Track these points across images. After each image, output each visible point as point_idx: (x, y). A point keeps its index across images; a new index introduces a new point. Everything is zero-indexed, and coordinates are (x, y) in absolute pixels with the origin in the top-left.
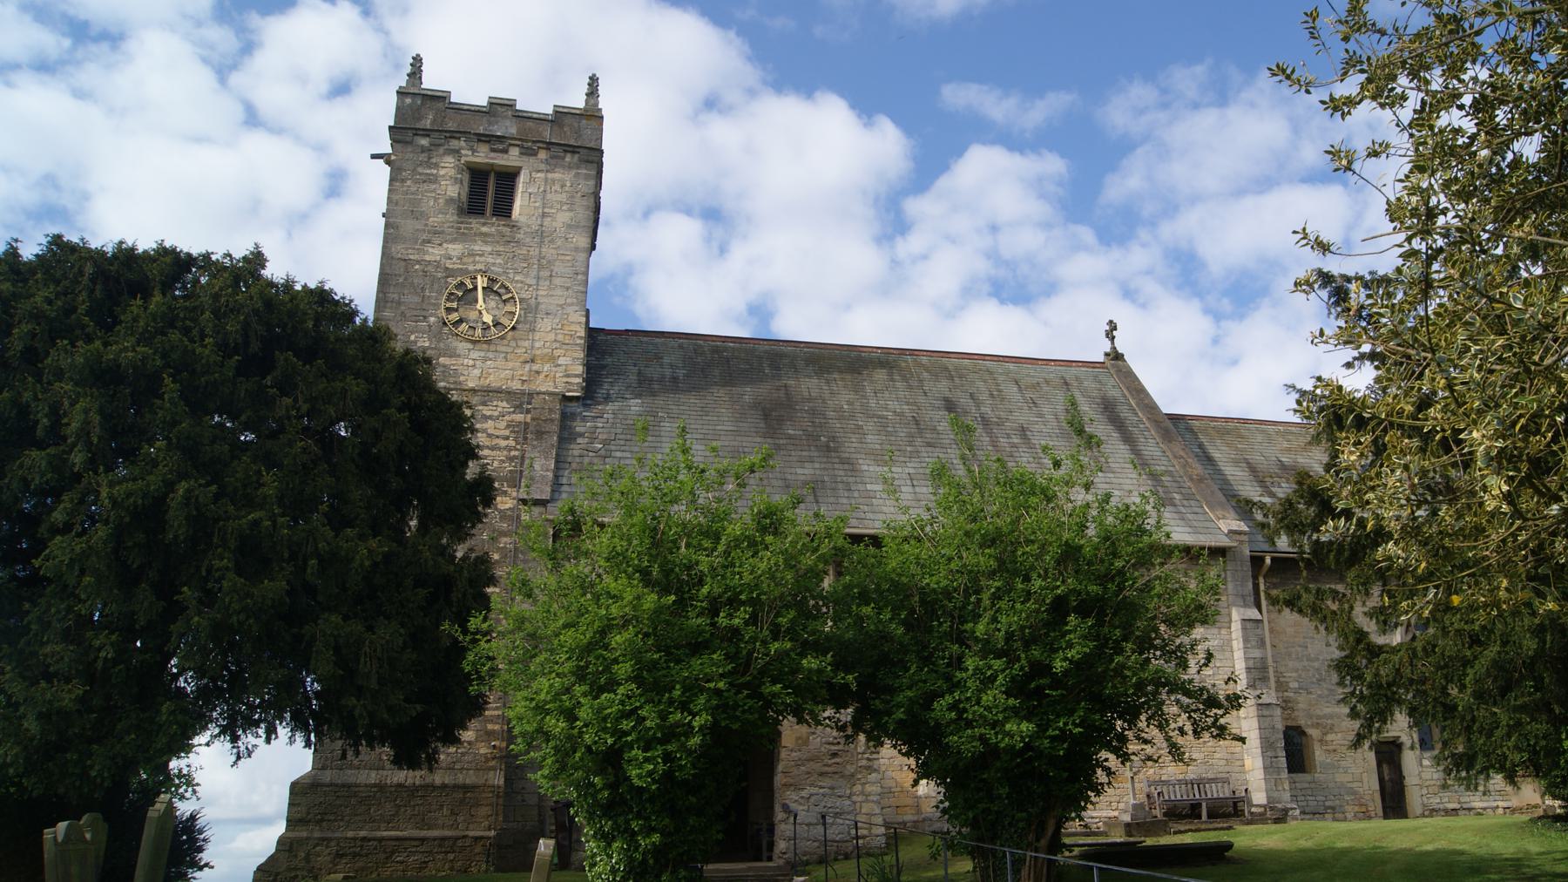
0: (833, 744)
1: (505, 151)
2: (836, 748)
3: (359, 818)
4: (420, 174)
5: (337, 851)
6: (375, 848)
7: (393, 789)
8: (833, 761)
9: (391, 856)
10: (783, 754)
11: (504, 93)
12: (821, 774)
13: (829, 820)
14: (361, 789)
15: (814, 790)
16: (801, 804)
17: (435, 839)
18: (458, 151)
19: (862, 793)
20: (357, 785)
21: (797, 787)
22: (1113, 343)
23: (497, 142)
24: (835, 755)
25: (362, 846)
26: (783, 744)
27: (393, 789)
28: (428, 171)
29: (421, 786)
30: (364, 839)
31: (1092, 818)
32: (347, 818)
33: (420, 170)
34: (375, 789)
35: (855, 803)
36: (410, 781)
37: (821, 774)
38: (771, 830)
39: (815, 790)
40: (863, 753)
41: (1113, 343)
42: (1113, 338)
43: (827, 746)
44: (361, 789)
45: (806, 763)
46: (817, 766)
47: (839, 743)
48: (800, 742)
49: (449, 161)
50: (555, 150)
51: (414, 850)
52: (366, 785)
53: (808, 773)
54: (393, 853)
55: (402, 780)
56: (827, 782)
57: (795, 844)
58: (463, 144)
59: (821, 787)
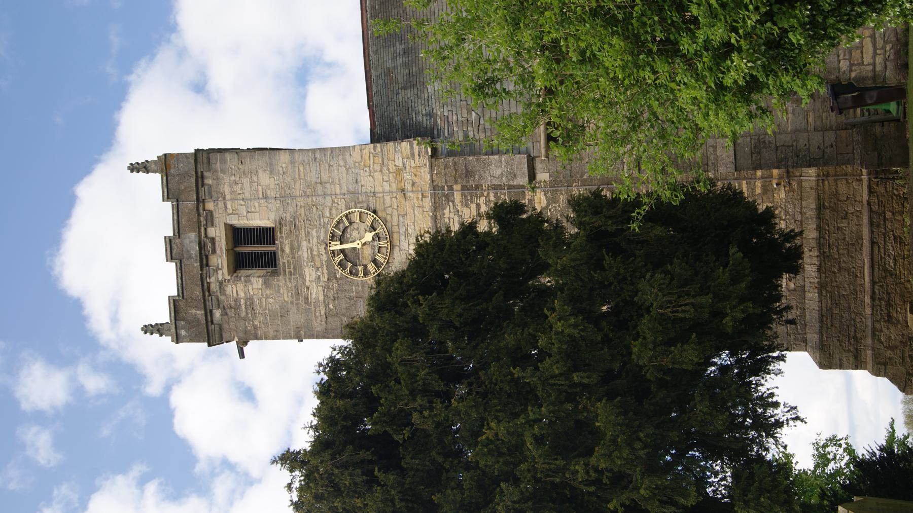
1: (213, 240)
3: (852, 305)
4: (247, 313)
6: (882, 286)
9: (890, 272)
14: (824, 305)
17: (872, 232)
18: (221, 283)
28: (243, 307)
29: (819, 250)
30: (873, 298)
32: (853, 315)
33: (243, 314)
44: (824, 305)
49: (230, 289)
51: (882, 251)
52: (821, 301)
54: (886, 270)
55: (814, 268)
58: (213, 279)
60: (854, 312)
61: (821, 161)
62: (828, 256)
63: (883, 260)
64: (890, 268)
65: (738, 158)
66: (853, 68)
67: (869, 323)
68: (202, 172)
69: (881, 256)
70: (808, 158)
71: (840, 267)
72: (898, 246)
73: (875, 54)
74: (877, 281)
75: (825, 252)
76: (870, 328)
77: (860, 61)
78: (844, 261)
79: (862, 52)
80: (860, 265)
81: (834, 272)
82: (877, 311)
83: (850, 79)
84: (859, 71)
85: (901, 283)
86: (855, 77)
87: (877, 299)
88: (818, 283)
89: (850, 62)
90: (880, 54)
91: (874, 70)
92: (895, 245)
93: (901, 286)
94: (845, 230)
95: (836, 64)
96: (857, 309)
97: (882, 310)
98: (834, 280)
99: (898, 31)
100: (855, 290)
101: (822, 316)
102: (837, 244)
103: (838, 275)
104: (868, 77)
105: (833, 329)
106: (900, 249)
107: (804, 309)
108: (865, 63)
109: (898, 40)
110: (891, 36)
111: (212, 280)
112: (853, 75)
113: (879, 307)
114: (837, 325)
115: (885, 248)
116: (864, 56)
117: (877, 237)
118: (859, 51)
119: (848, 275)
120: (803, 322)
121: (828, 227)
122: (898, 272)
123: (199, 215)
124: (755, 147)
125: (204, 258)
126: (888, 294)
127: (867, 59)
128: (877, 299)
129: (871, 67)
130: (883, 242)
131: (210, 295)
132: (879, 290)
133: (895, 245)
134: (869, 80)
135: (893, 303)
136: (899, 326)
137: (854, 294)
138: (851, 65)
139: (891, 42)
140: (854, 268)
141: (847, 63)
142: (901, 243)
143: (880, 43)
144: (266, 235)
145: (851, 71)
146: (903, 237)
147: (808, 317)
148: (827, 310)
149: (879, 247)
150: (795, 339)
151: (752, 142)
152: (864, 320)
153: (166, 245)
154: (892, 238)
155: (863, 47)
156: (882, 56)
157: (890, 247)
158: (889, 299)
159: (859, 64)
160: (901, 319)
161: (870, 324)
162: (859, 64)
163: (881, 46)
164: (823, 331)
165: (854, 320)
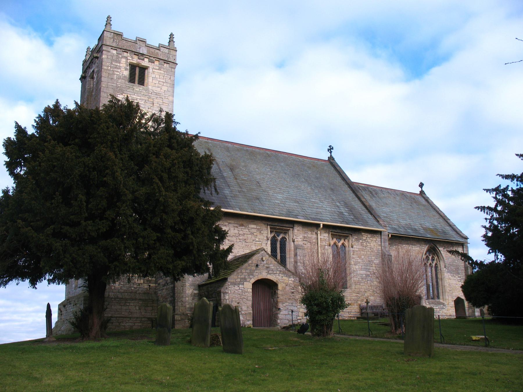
0: (292, 289)
1: (143, 60)
2: (293, 290)
4: (114, 65)
11: (142, 36)
15: (287, 304)
18: (127, 57)
22: (331, 154)
23: (141, 55)
24: (293, 293)
28: (116, 64)
31: (344, 316)
41: (331, 154)
42: (331, 152)
47: (294, 289)
49: (123, 60)
50: (161, 61)
58: (129, 55)
68: (169, 64)
111: (128, 54)
123: (154, 57)
125: (138, 54)
131: (123, 51)
144: (142, 82)
153: (117, 31)
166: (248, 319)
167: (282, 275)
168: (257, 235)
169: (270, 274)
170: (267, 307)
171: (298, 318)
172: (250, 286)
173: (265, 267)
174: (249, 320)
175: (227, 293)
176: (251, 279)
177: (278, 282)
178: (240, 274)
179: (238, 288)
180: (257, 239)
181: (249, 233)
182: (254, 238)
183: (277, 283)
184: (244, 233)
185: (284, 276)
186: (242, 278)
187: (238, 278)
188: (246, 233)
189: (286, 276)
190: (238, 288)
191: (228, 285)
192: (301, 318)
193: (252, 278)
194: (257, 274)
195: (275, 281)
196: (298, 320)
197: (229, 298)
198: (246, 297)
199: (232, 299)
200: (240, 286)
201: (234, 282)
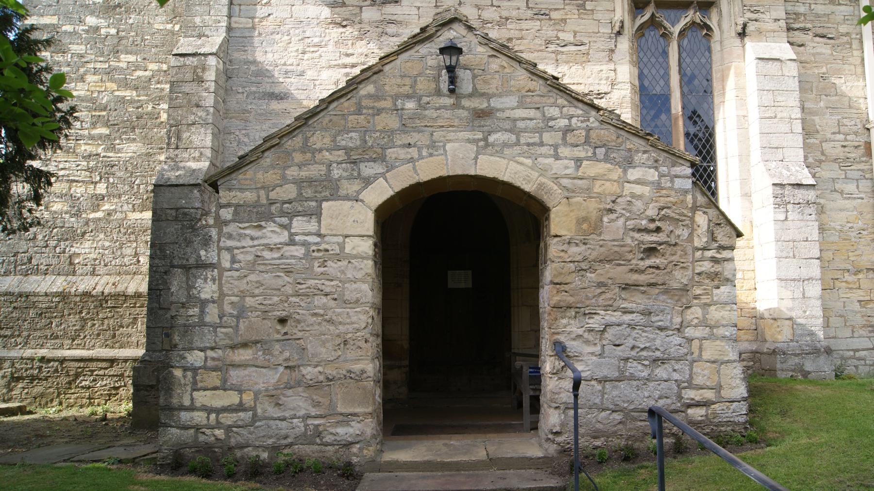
0: (646, 231)
2: (654, 238)
3: (38, 334)
5: (12, 374)
6: (56, 371)
7: (78, 299)
8: (648, 262)
9: (74, 380)
10: (554, 249)
12: (626, 287)
13: (402, 74)
14: (41, 299)
15: (614, 317)
16: (587, 342)
17: (126, 361)
19: (704, 323)
20: (36, 295)
21: (582, 312)
24: (651, 251)
25: (40, 368)
26: (553, 232)
27: (78, 299)
29: (110, 294)
30: (42, 359)
32: (25, 334)
34: (57, 299)
35: (690, 340)
36: (99, 289)
37: (626, 287)
38: (536, 378)
39: (614, 317)
40: (704, 249)
43: (637, 235)
44: (41, 299)
45: (596, 266)
46: (620, 273)
47: (658, 230)
48: (585, 226)
51: (101, 372)
52: (46, 295)
53: (600, 285)
54: (77, 375)
55: (89, 288)
56: (637, 301)
57: (576, 413)
59: (626, 312)
60: (29, 336)
61: (155, 305)
62: (101, 305)
63: (89, 373)
64: (78, 382)
65: (173, 189)
66: (189, 374)
67: (14, 353)
69: (95, 370)
70: (161, 287)
71: (87, 319)
72: (106, 392)
73: (209, 410)
74: (64, 366)
75: (107, 302)
76: (5, 355)
77: (200, 385)
78: (94, 325)
79: (215, 388)
80: (87, 344)
81: (81, 312)
82: (26, 364)
83: (172, 367)
84: (183, 382)
85: (59, 394)
86: (173, 376)
87: (41, 364)
88: (70, 292)
89: (200, 368)
90: (208, 418)
91: (182, 408)
92: (107, 388)
93: (56, 395)
94: (132, 328)
95: (199, 344)
96: (34, 338)
97: (26, 370)
98: (71, 311)
99: (246, 450)
100: (57, 337)
101: (27, 296)
102: (115, 317)
103: (77, 316)
104: (171, 397)
105: (10, 309)
106: (102, 395)
107: (46, 274)
108: (195, 394)
109: (230, 449)
110: (239, 438)
112: (178, 373)
113: (30, 366)
114: (14, 315)
115: (104, 375)
116: (208, 393)
117: (120, 366)
118: (218, 383)
119: (76, 330)
120: (29, 272)
121: (139, 307)
122: (73, 391)
124: (185, 214)
126: (46, 379)
127: (202, 398)
128: (41, 364)
129: (187, 402)
130: (112, 373)
132: (53, 367)
133: (107, 388)
134: (166, 399)
135: (35, 384)
136: (5, 391)
137: (51, 336)
138: (195, 370)
139: (228, 437)
140: (85, 337)
141: (199, 364)
142: (110, 395)
143: (228, 419)
145: (185, 369)
146: (116, 398)
147: (35, 277)
148: (34, 303)
149: (106, 369)
150: (9, 261)
151: (192, 210)
152: (20, 346)
154: (117, 385)
155: (225, 390)
156: (205, 422)
157: (104, 382)
158: (40, 379)
159: (195, 383)
160: (14, 393)
161: (10, 355)
162: (195, 383)
163: (222, 421)
164: (8, 297)
165: (19, 336)
166: (340, 409)
167: (580, 152)
168: (564, 21)
169: (500, 149)
170: (87, 462)
171: (690, 394)
172: (367, 223)
173: (464, 114)
174: (347, 418)
175: (212, 266)
176: (368, 182)
177: (549, 192)
178: (298, 157)
179: (284, 236)
180: (567, 37)
181: (529, 13)
182: (550, 33)
183: (545, 198)
184: (505, 14)
185: (594, 158)
186: (310, 181)
187: (284, 180)
188: (514, 13)
189: (607, 159)
190: (284, 236)
191: (220, 223)
192: (709, 395)
193: (376, 177)
194: (413, 152)
195: (527, 187)
196: (689, 406)
197: (222, 295)
198: (329, 286)
199: (243, 297)
200: (298, 224)
201: (256, 204)
